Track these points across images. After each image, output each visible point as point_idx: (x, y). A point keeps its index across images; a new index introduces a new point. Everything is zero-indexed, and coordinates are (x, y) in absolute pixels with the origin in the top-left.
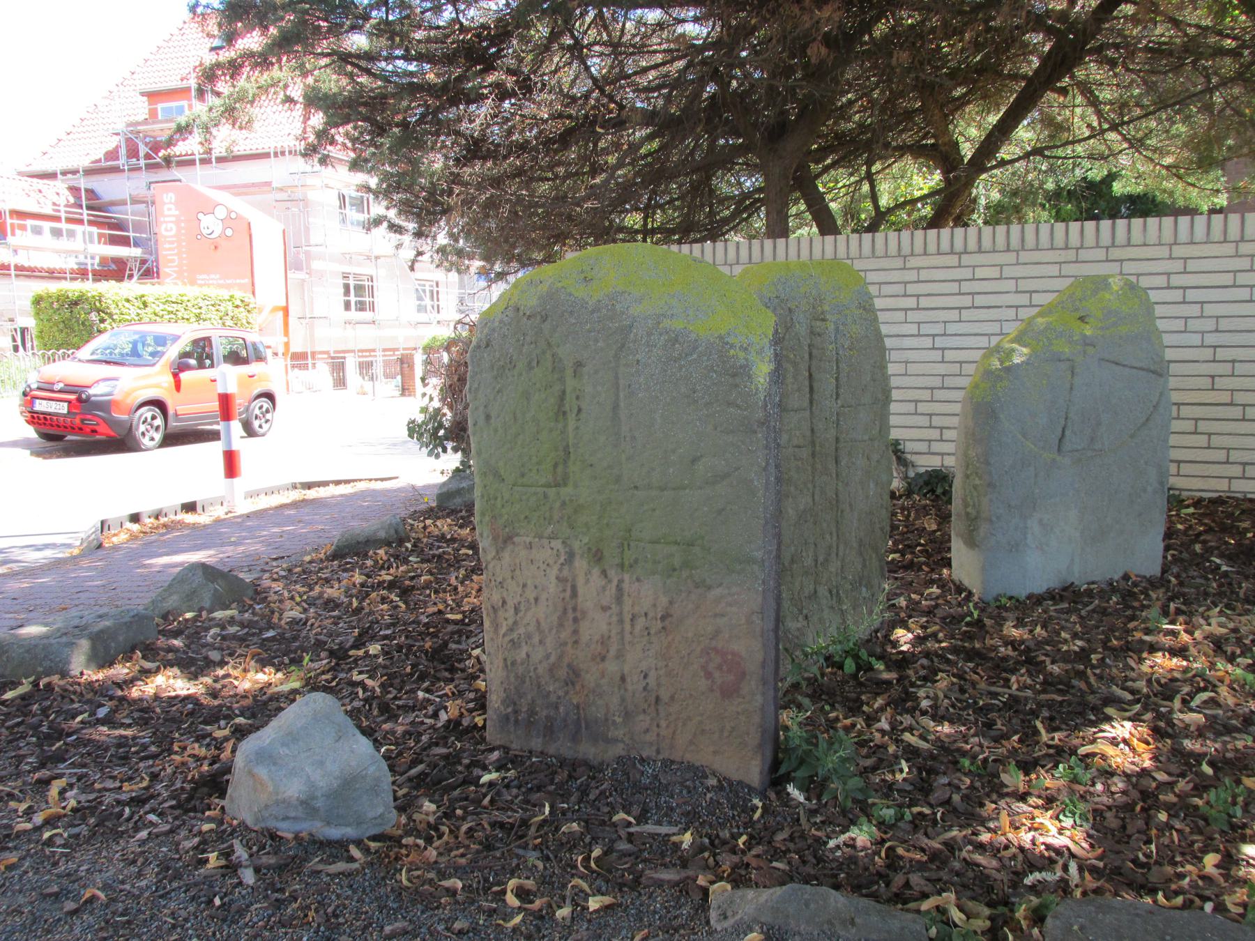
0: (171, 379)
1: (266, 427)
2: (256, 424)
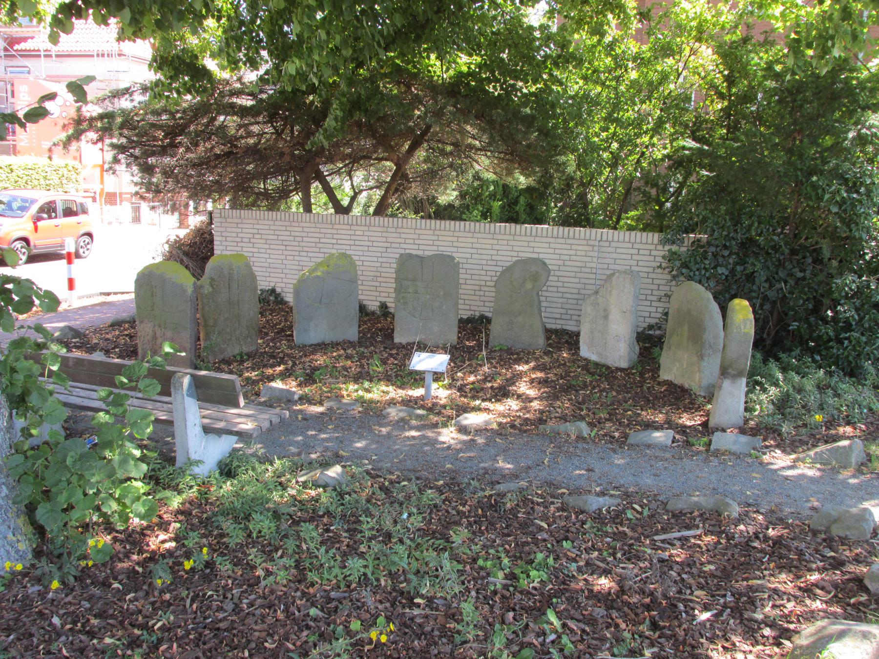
0: (32, 225)
1: (87, 252)
2: (81, 251)
